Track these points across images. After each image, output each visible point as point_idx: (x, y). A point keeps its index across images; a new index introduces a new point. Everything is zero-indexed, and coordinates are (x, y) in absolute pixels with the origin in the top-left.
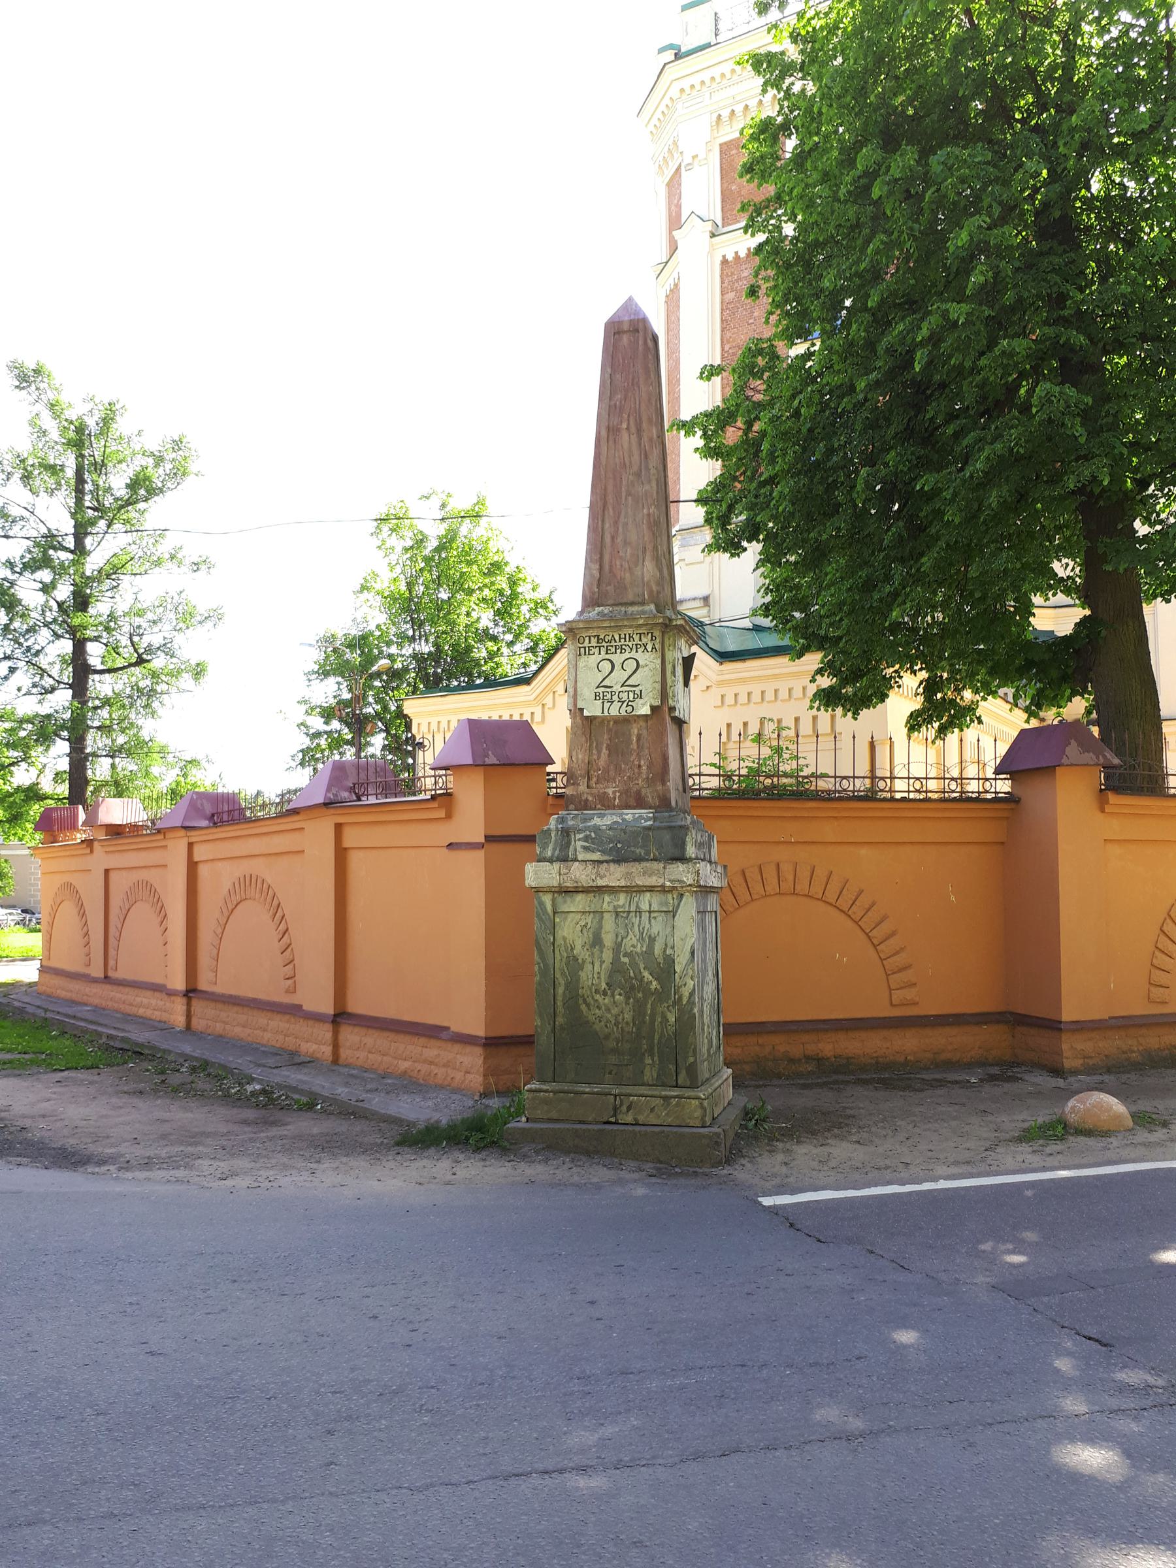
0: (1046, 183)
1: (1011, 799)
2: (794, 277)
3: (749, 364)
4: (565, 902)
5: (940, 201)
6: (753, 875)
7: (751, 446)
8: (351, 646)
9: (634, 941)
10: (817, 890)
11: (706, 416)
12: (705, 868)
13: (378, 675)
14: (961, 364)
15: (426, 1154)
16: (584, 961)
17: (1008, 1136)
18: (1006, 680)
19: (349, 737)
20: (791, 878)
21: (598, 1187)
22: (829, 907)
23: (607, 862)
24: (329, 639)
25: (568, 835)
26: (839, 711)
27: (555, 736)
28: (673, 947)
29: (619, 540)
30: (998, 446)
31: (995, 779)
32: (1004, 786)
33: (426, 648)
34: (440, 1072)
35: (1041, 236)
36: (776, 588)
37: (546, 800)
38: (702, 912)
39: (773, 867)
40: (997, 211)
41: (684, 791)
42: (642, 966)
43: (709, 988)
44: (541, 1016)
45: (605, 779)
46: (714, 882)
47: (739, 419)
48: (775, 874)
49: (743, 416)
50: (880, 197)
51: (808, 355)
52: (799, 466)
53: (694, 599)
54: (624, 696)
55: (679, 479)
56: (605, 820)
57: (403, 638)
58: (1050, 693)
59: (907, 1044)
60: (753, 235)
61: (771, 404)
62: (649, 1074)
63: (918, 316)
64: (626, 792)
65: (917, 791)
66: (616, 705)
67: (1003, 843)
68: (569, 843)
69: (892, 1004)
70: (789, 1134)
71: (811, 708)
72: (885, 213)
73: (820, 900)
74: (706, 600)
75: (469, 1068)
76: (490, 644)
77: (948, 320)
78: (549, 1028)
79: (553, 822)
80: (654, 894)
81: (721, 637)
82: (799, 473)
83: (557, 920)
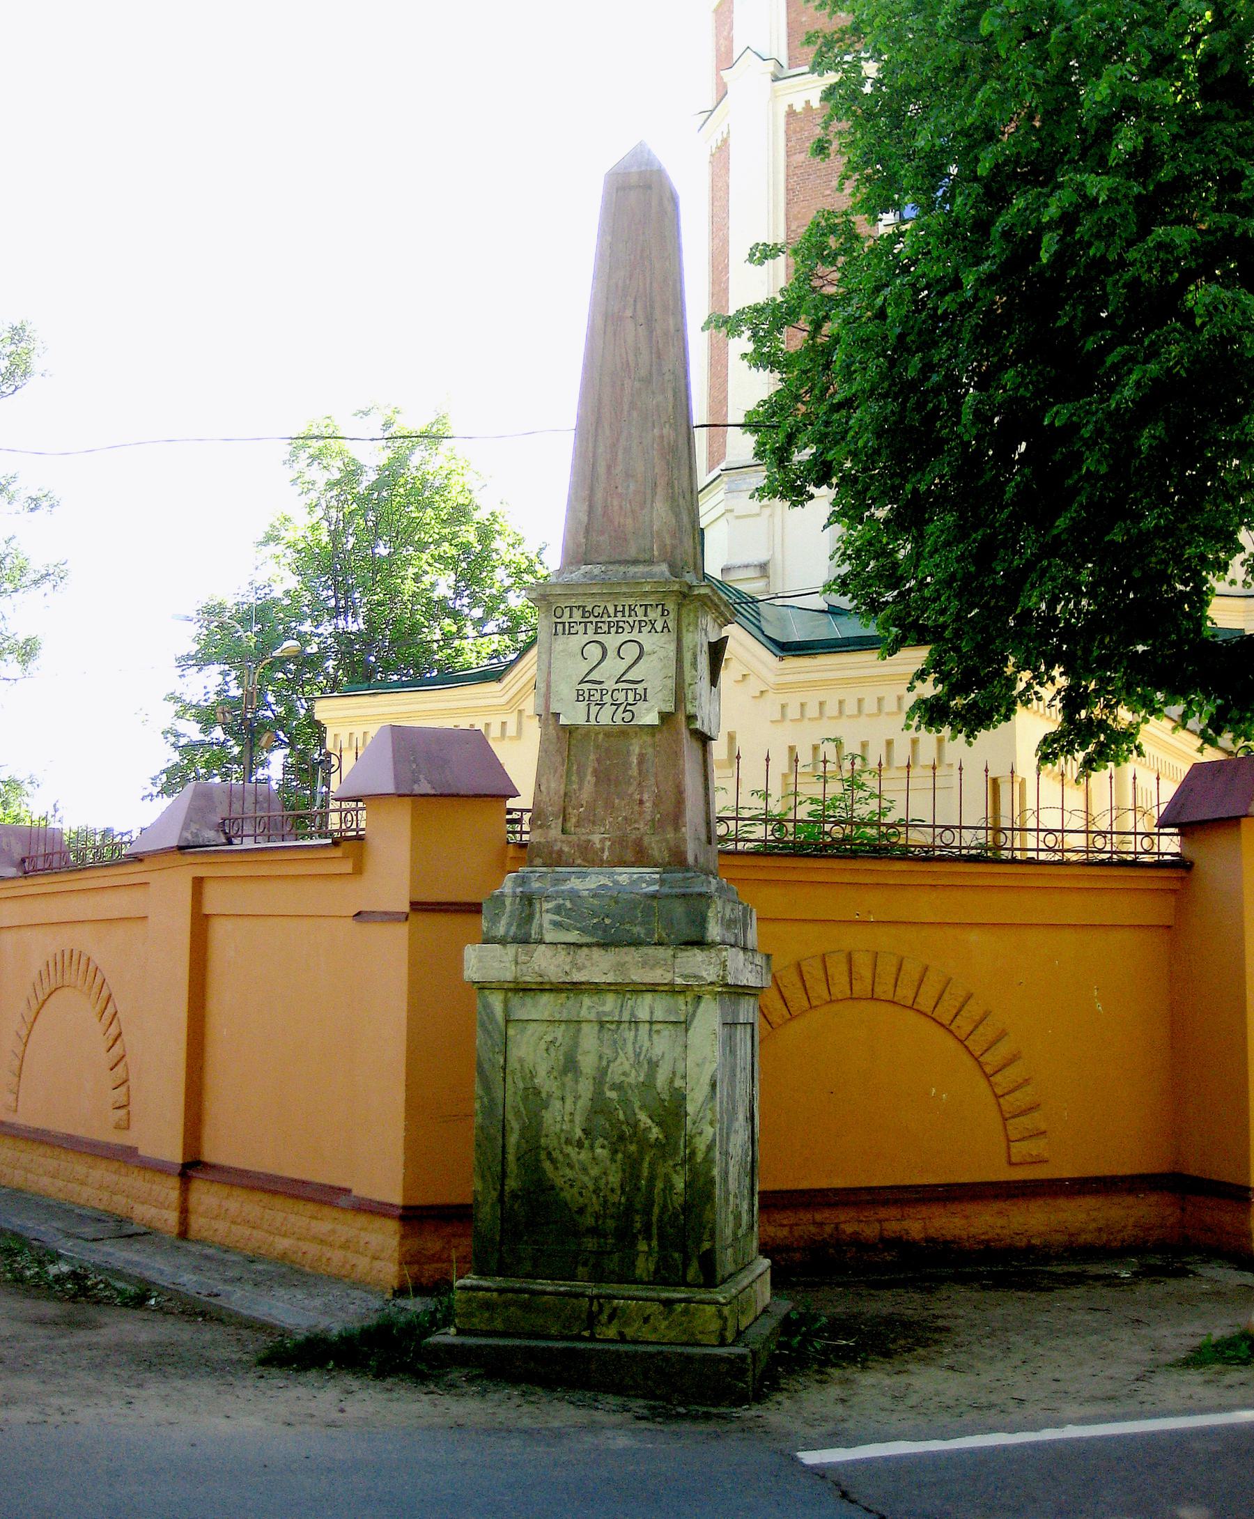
0: (1209, 29)
1: (1181, 864)
2: (879, 135)
3: (819, 244)
4: (523, 1005)
5: (1070, 45)
6: (813, 971)
7: (821, 355)
8: (245, 620)
9: (627, 1067)
10: (905, 993)
11: (757, 310)
12: (736, 959)
13: (281, 663)
14: (1103, 257)
15: (302, 1379)
16: (549, 1096)
17: (1169, 1358)
18: (1177, 690)
19: (236, 750)
20: (867, 974)
21: (559, 1435)
22: (923, 1020)
23: (588, 945)
24: (212, 611)
25: (531, 904)
26: (946, 731)
27: (521, 761)
28: (684, 1077)
29: (619, 469)
30: (1153, 367)
31: (1159, 834)
32: (1170, 845)
33: (355, 625)
34: (337, 1256)
35: (1205, 95)
36: (853, 553)
37: (503, 853)
38: (731, 1025)
39: (842, 958)
40: (1146, 60)
41: (709, 842)
42: (637, 1104)
43: (739, 1139)
44: (483, 1177)
45: (591, 819)
46: (749, 978)
47: (803, 317)
48: (845, 968)
49: (808, 314)
50: (991, 34)
51: (898, 236)
52: (886, 385)
53: (747, 566)
54: (620, 697)
55: (726, 398)
56: (586, 883)
57: (318, 612)
58: (1235, 714)
59: (1032, 1221)
60: (821, 75)
61: (846, 298)
62: (644, 1266)
63: (1045, 190)
64: (620, 842)
65: (1050, 849)
66: (608, 710)
67: (1169, 927)
68: (531, 917)
69: (1011, 1164)
70: (849, 1357)
71: (908, 727)
72: (998, 56)
73: (911, 1008)
74: (763, 568)
75: (378, 1252)
76: (448, 625)
77: (1084, 197)
78: (494, 1194)
79: (508, 885)
80: (657, 996)
81: (782, 621)
82: (885, 396)
83: (511, 1032)
